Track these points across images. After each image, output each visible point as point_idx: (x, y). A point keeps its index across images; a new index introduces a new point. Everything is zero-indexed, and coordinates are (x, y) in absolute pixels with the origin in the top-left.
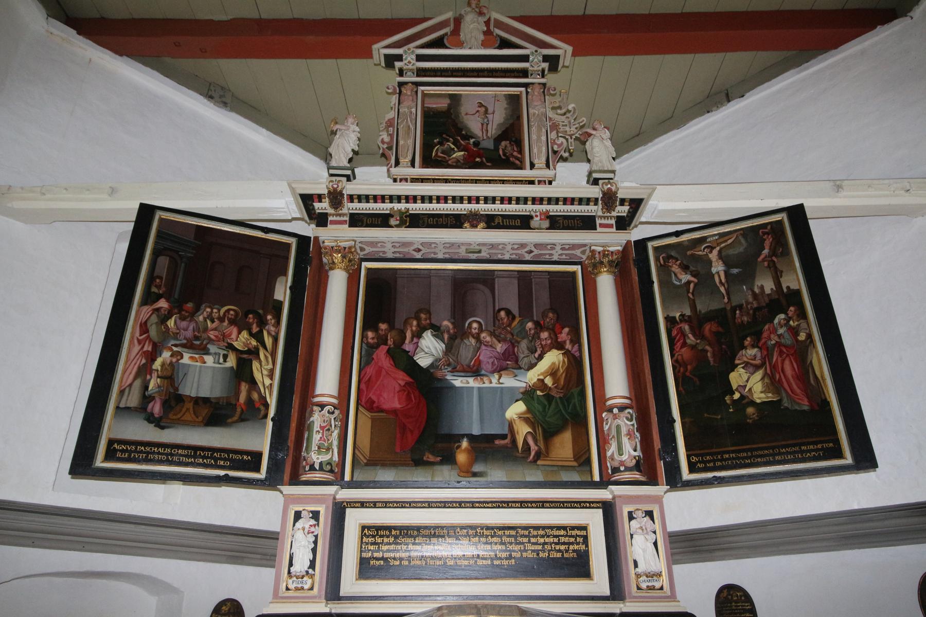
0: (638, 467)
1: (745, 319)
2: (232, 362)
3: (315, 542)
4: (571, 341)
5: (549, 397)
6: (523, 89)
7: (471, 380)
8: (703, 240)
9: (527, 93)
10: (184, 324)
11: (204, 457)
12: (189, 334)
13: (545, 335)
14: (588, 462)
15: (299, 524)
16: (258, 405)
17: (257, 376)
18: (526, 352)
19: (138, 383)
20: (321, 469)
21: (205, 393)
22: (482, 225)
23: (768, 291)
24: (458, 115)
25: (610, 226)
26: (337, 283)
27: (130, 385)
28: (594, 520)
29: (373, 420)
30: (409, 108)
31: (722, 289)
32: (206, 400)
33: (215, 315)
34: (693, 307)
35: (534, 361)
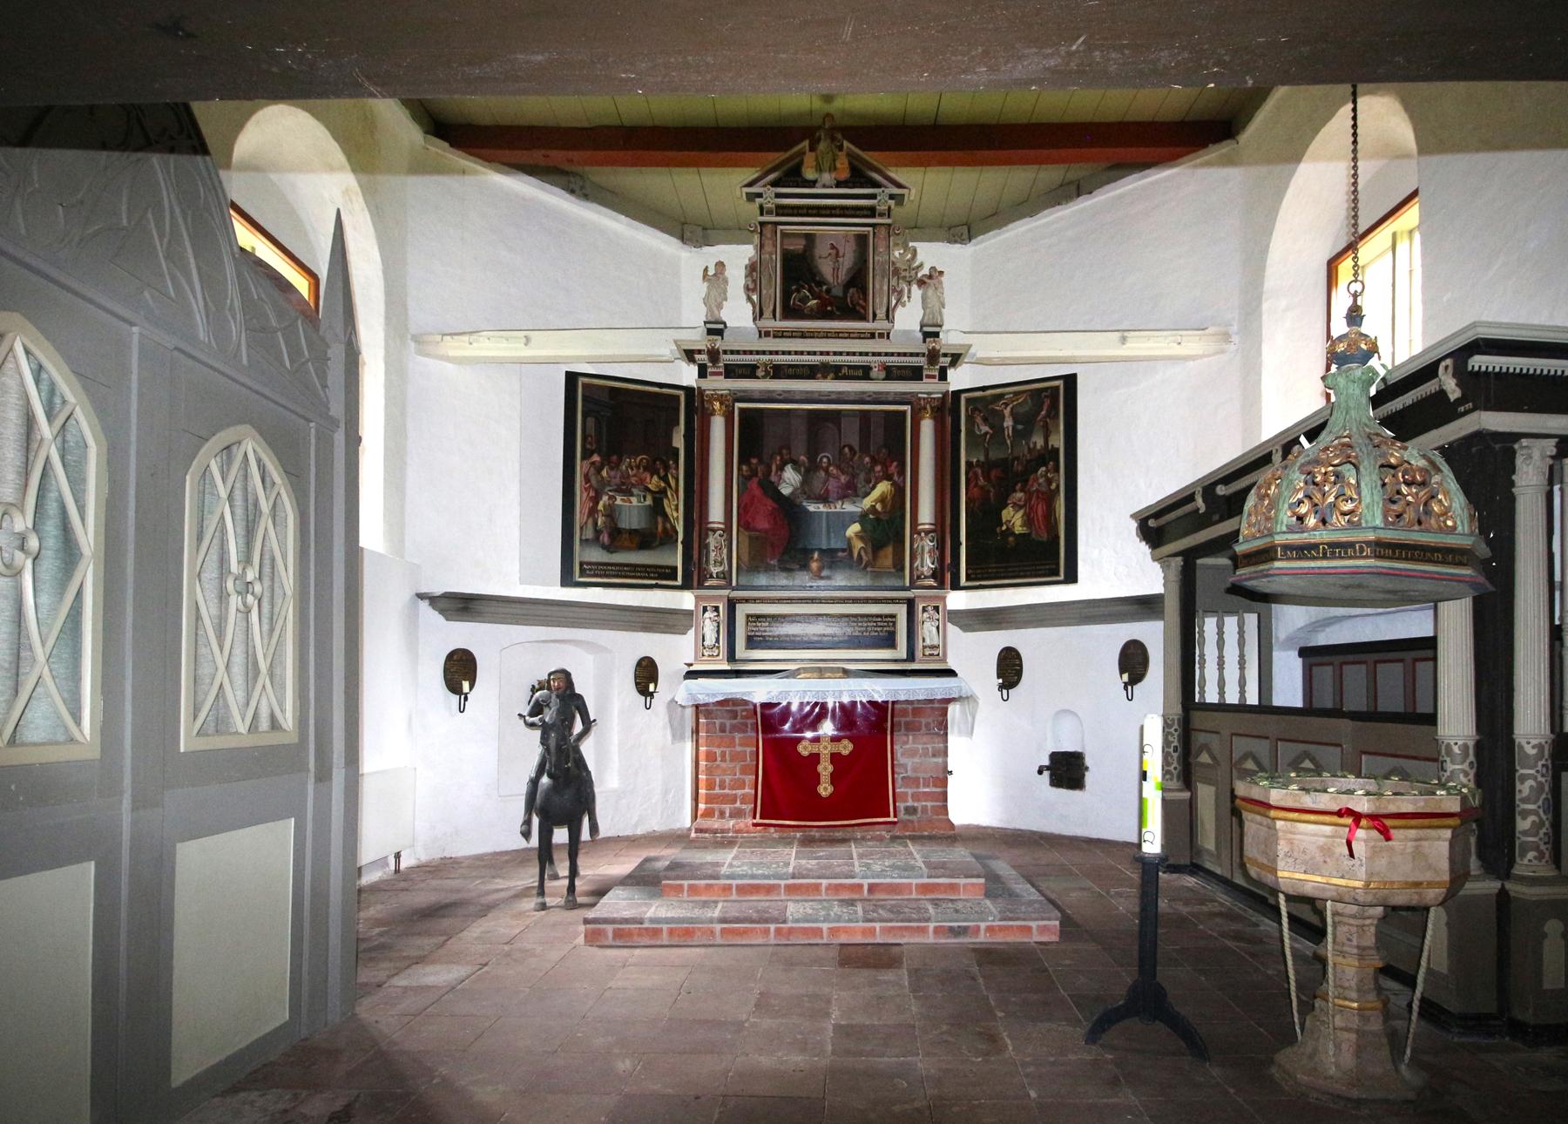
0: (934, 575)
1: (1020, 468)
2: (649, 501)
3: (718, 627)
4: (898, 473)
5: (878, 520)
6: (870, 229)
7: (821, 506)
8: (1001, 396)
9: (874, 233)
10: (612, 473)
11: (641, 572)
12: (617, 480)
13: (878, 468)
14: (903, 569)
15: (707, 615)
16: (671, 532)
17: (668, 510)
18: (863, 483)
19: (590, 521)
20: (717, 577)
21: (635, 526)
22: (832, 375)
23: (1038, 447)
24: (812, 257)
25: (934, 377)
26: (718, 426)
27: (586, 523)
28: (901, 611)
29: (750, 537)
30: (771, 254)
31: (1009, 442)
32: (635, 530)
33: (633, 464)
34: (987, 456)
35: (868, 491)
